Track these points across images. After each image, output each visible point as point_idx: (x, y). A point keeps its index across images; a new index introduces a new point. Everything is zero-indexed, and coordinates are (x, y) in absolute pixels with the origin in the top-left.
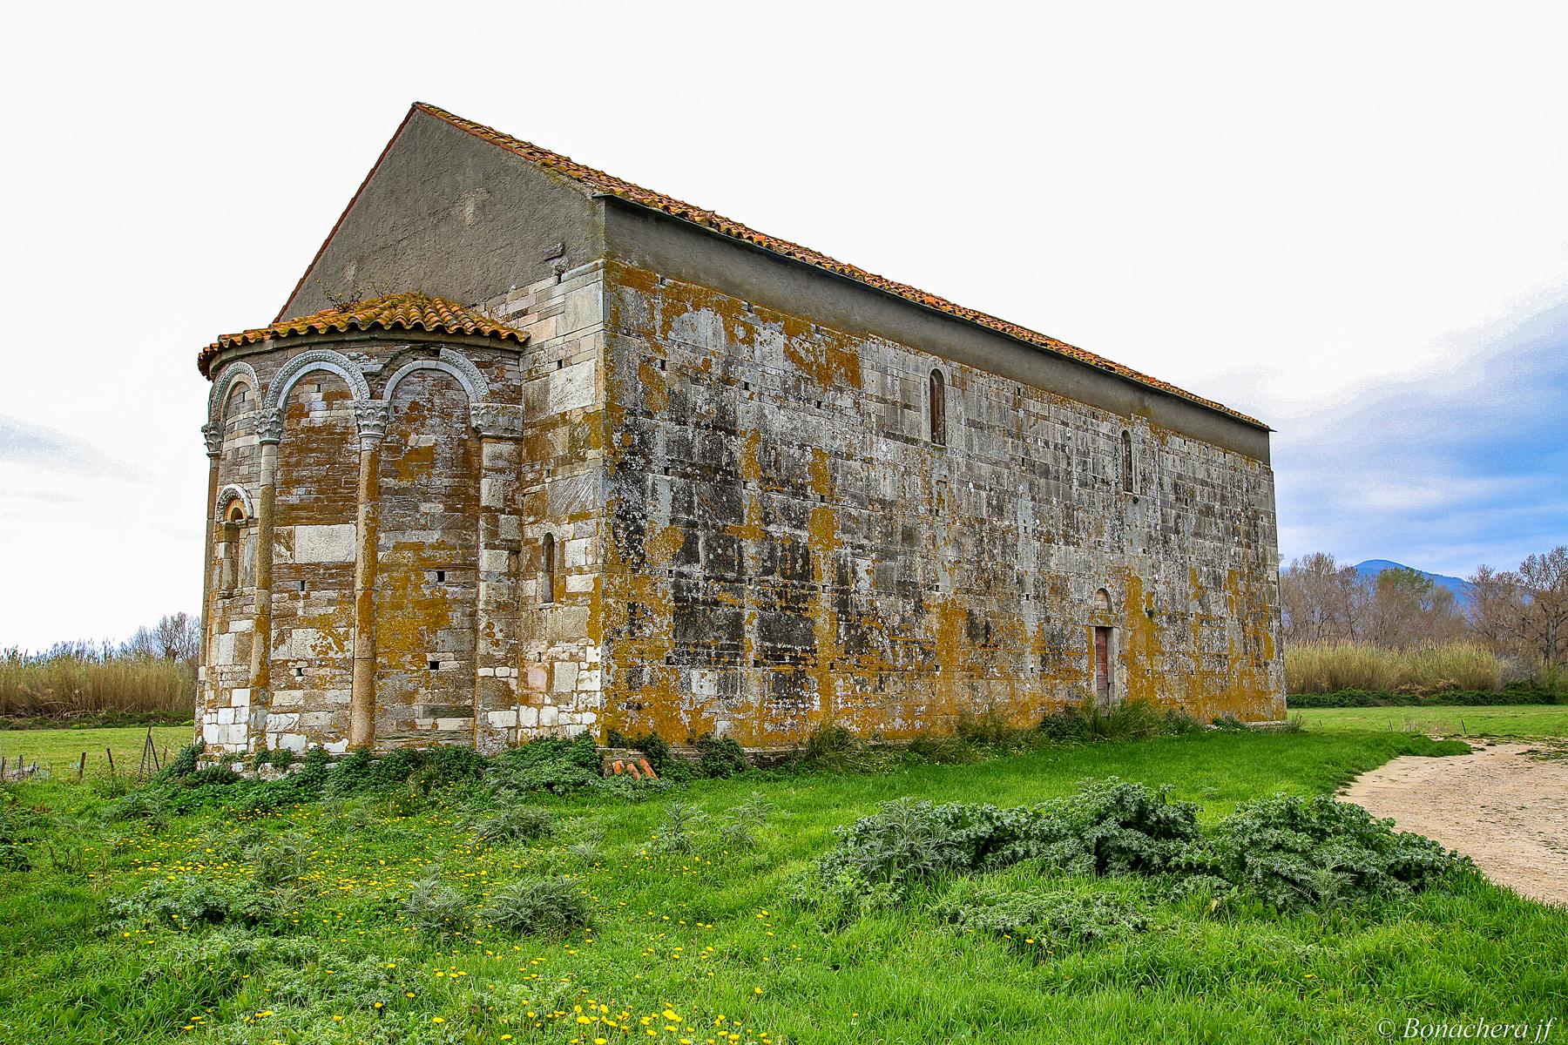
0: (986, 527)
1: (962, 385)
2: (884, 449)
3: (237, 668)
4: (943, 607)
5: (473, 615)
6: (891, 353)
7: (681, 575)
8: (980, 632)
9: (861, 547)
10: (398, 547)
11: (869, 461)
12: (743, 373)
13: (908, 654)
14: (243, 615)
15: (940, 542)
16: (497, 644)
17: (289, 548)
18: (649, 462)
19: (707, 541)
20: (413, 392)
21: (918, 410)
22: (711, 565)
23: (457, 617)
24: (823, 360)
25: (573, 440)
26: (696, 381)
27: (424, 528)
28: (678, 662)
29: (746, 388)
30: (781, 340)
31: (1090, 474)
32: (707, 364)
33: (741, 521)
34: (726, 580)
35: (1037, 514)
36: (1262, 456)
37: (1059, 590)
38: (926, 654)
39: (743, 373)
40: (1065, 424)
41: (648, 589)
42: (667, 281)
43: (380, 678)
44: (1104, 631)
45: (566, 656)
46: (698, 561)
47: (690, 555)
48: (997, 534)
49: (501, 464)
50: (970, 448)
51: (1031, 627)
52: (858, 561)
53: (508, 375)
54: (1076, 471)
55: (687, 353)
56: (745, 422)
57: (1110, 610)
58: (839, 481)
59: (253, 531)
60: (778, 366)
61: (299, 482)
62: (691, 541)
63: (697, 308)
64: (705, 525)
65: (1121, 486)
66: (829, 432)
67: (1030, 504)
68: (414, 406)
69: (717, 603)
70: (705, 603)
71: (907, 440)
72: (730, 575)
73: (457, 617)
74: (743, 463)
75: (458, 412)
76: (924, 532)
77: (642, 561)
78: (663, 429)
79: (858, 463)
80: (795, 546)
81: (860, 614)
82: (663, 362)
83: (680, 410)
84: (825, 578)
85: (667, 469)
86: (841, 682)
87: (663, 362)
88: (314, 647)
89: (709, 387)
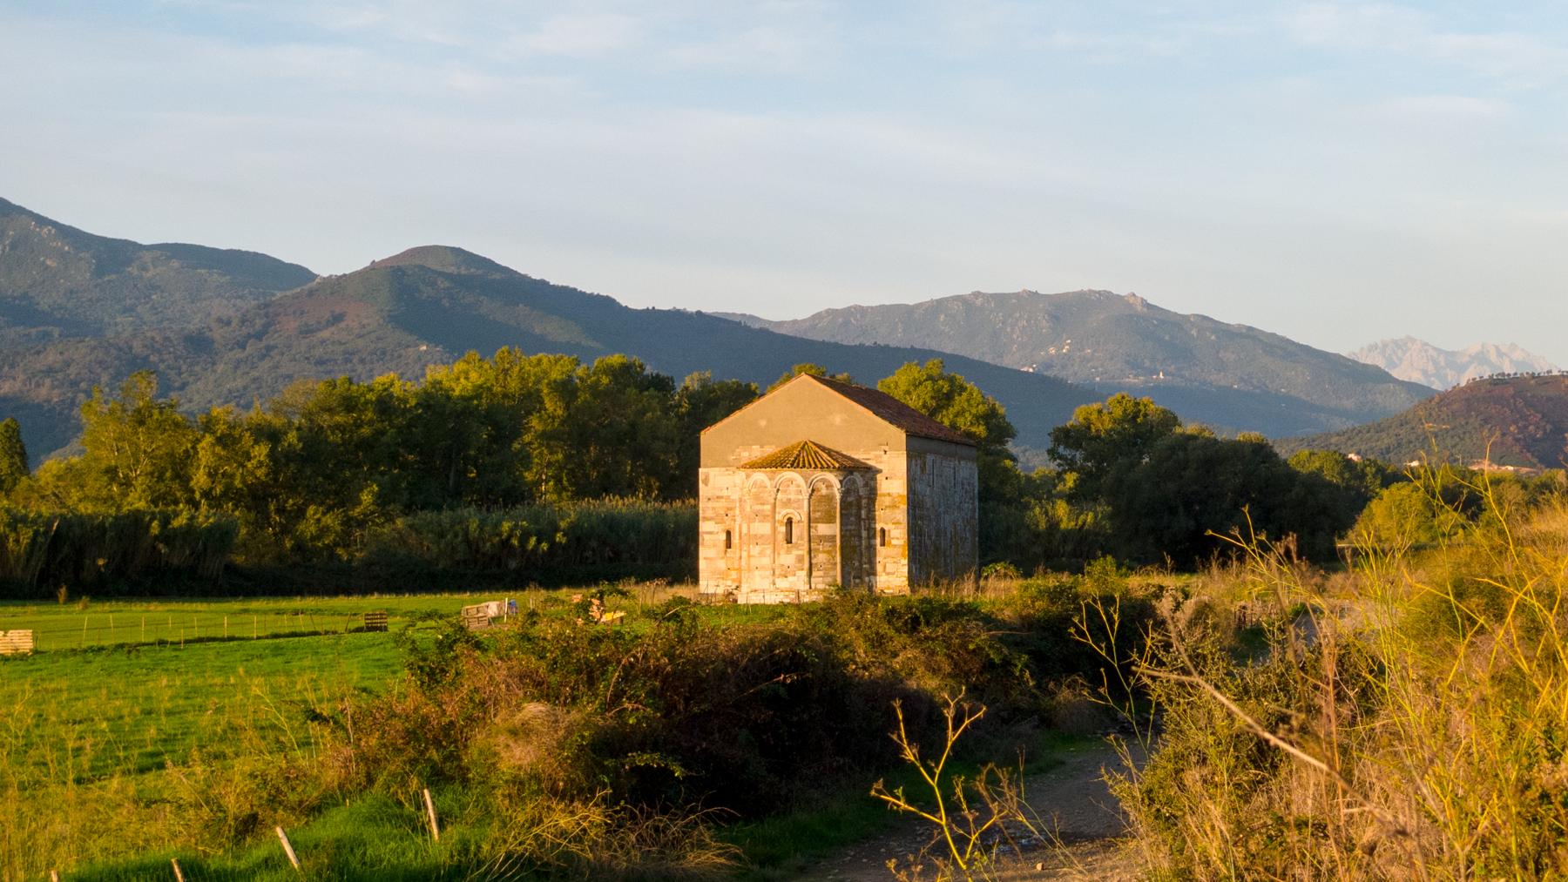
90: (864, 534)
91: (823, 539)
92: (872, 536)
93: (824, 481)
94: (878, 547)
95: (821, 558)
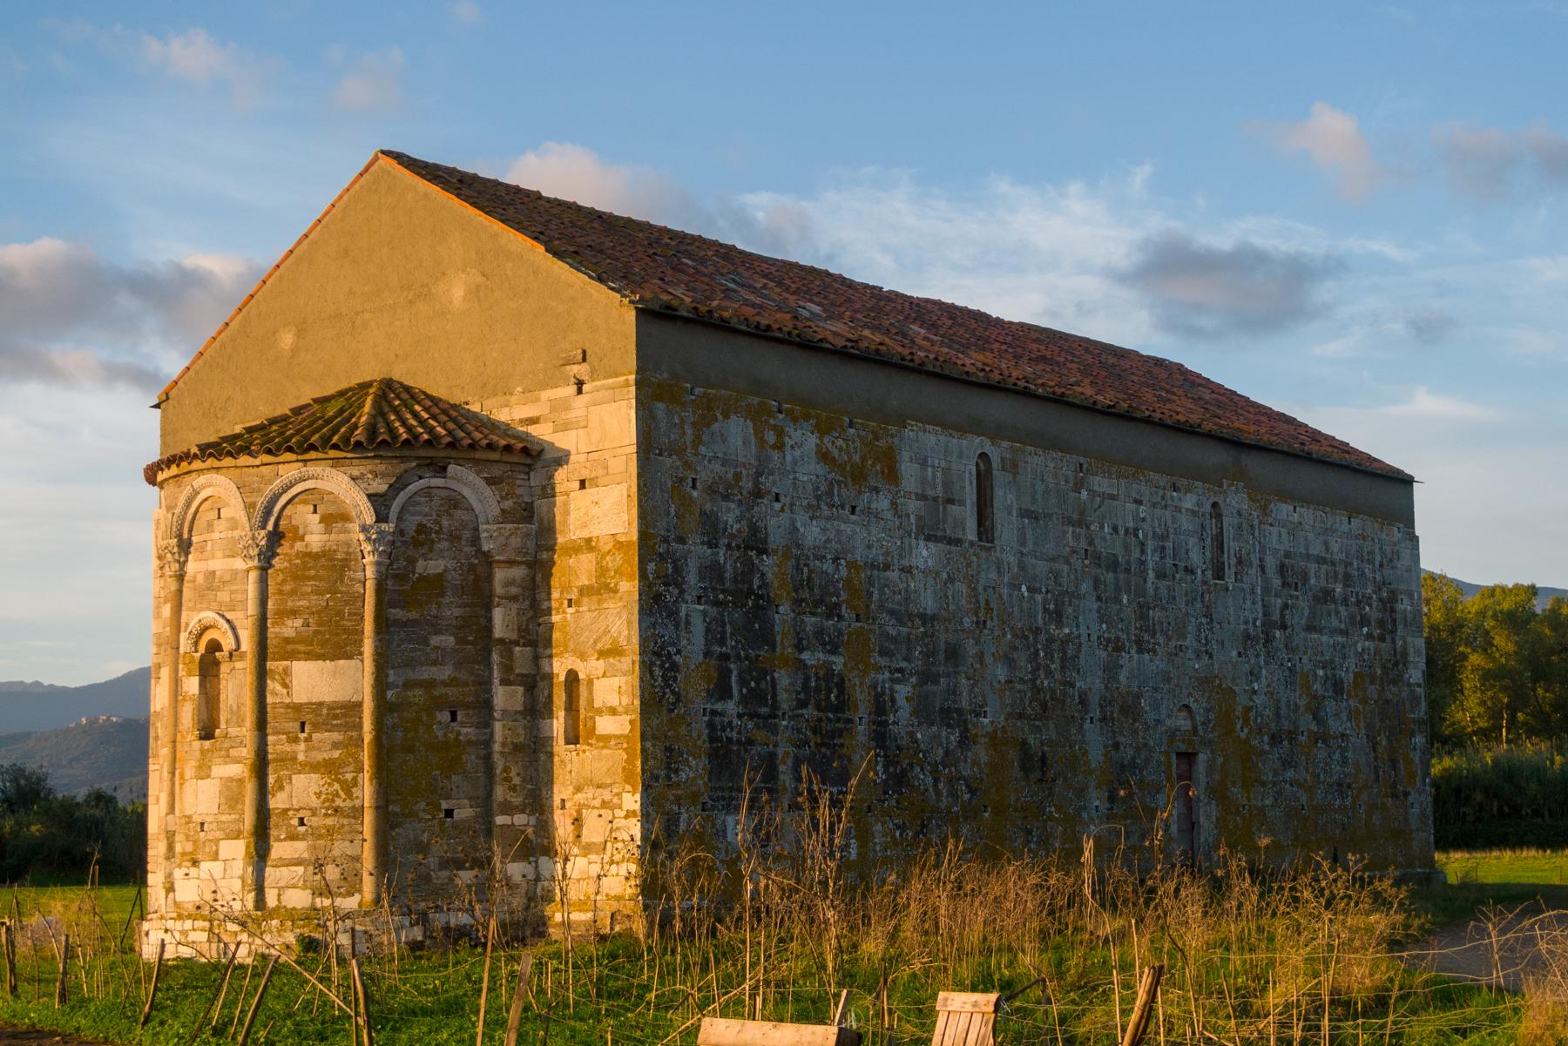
0: (1042, 637)
1: (1012, 467)
2: (925, 554)
3: (224, 818)
4: (992, 736)
5: (488, 758)
6: (931, 439)
7: (714, 713)
8: (1035, 764)
9: (900, 670)
10: (408, 685)
11: (907, 570)
12: (774, 483)
13: (953, 794)
14: (228, 759)
15: (988, 659)
16: (514, 790)
17: (285, 686)
18: (682, 592)
19: (739, 675)
20: (419, 514)
21: (962, 503)
22: (744, 700)
23: (471, 759)
24: (857, 458)
25: (602, 571)
26: (726, 498)
27: (435, 663)
28: (714, 808)
29: (777, 500)
30: (813, 440)
31: (1169, 561)
32: (738, 477)
33: (774, 650)
34: (759, 716)
35: (1102, 618)
36: (1404, 517)
37: (1130, 709)
38: (972, 791)
39: (774, 483)
40: (1138, 502)
41: (683, 730)
42: (698, 390)
43: (392, 828)
44: (1188, 757)
45: (597, 803)
46: (731, 697)
47: (723, 692)
48: (1056, 646)
49: (514, 590)
50: (1023, 542)
51: (1096, 756)
52: (897, 687)
53: (519, 491)
54: (1152, 559)
55: (717, 467)
56: (776, 535)
57: (1195, 730)
58: (876, 596)
59: (239, 665)
60: (810, 471)
61: (294, 613)
62: (725, 675)
63: (726, 416)
64: (738, 657)
65: (1209, 574)
66: (864, 538)
67: (1095, 606)
68: (421, 528)
69: (750, 742)
70: (739, 742)
71: (951, 541)
72: (764, 710)
73: (471, 759)
74: (776, 585)
75: (467, 534)
76: (971, 649)
77: (678, 700)
78: (696, 552)
79: (897, 573)
80: (830, 673)
81: (899, 748)
82: (694, 480)
83: (712, 530)
84: (862, 711)
85: (699, 598)
86: (879, 827)
87: (694, 480)
88: (318, 795)
89: (740, 503)
90: (505, 697)
91: (309, 717)
92: (536, 710)
93: (314, 498)
94: (560, 747)
95: (299, 791)
